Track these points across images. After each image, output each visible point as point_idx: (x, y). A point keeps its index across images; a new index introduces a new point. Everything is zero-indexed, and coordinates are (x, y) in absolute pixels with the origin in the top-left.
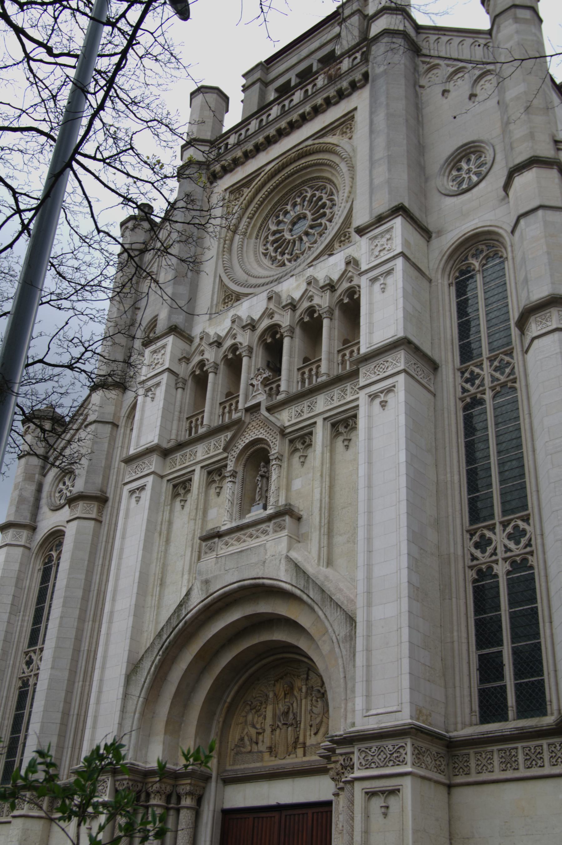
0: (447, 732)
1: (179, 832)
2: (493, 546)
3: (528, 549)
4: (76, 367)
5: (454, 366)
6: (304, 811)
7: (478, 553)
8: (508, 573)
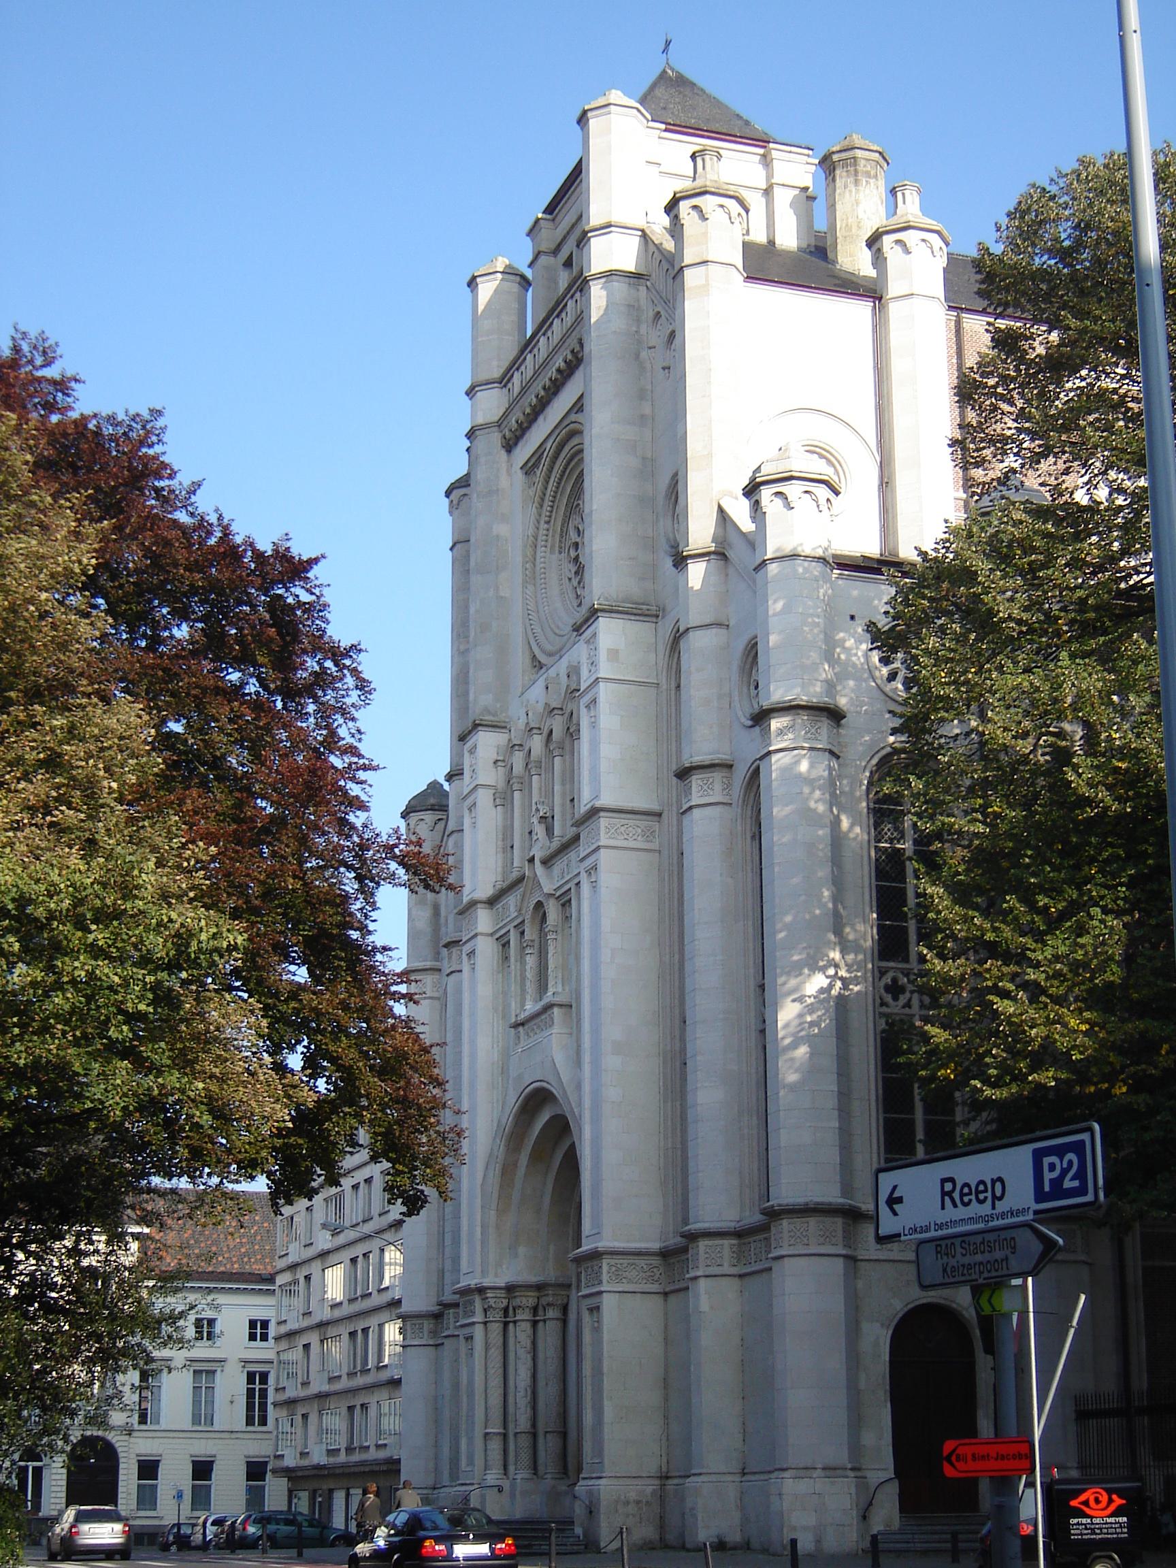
6: (718, 1242)
7: (888, 998)
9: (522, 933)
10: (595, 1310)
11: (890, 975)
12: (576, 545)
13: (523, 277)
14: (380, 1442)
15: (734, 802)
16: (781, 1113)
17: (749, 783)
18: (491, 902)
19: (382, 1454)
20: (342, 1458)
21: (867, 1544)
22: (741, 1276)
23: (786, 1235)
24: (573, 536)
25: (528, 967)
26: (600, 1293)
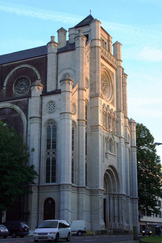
0: (91, 188)
3: (55, 156)
5: (100, 126)
7: (47, 155)
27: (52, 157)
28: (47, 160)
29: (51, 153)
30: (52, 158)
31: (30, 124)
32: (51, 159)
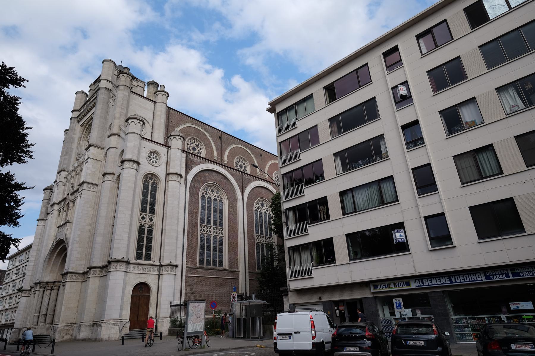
1: (165, 253)
2: (145, 219)
4: (277, 261)
6: (96, 269)
7: (141, 220)
8: (148, 227)
9: (64, 209)
10: (64, 286)
11: (143, 215)
12: (89, 139)
13: (87, 94)
14: (6, 320)
15: (114, 181)
16: (115, 240)
17: (118, 176)
18: (58, 204)
19: (11, 322)
20: (8, 322)
21: (121, 338)
22: (100, 277)
23: (112, 266)
24: (89, 138)
25: (63, 216)
26: (66, 282)
27: (148, 224)
28: (140, 226)
29: (147, 218)
30: (148, 225)
31: (103, 182)
32: (146, 226)
